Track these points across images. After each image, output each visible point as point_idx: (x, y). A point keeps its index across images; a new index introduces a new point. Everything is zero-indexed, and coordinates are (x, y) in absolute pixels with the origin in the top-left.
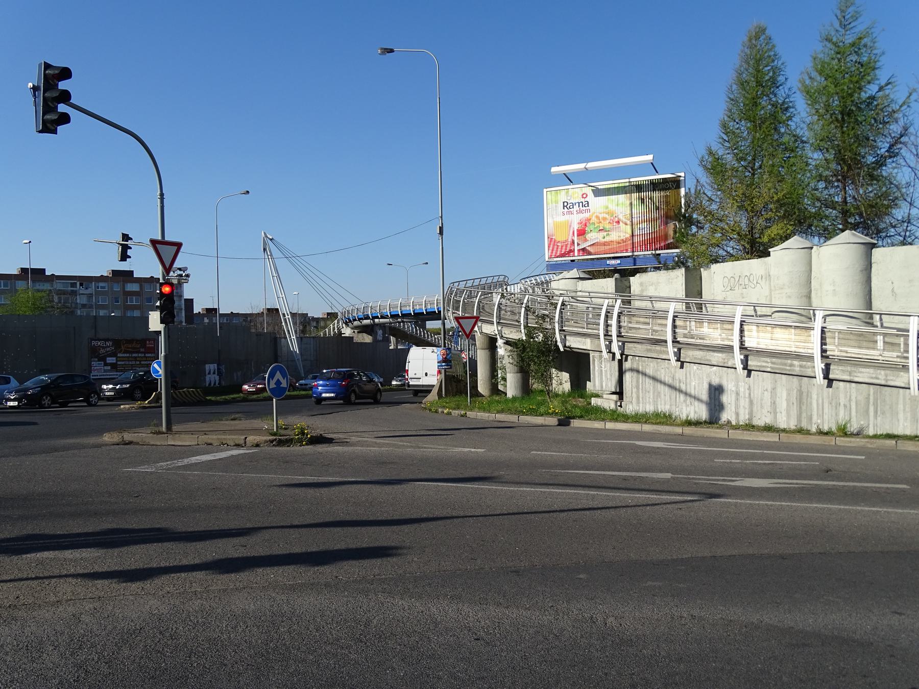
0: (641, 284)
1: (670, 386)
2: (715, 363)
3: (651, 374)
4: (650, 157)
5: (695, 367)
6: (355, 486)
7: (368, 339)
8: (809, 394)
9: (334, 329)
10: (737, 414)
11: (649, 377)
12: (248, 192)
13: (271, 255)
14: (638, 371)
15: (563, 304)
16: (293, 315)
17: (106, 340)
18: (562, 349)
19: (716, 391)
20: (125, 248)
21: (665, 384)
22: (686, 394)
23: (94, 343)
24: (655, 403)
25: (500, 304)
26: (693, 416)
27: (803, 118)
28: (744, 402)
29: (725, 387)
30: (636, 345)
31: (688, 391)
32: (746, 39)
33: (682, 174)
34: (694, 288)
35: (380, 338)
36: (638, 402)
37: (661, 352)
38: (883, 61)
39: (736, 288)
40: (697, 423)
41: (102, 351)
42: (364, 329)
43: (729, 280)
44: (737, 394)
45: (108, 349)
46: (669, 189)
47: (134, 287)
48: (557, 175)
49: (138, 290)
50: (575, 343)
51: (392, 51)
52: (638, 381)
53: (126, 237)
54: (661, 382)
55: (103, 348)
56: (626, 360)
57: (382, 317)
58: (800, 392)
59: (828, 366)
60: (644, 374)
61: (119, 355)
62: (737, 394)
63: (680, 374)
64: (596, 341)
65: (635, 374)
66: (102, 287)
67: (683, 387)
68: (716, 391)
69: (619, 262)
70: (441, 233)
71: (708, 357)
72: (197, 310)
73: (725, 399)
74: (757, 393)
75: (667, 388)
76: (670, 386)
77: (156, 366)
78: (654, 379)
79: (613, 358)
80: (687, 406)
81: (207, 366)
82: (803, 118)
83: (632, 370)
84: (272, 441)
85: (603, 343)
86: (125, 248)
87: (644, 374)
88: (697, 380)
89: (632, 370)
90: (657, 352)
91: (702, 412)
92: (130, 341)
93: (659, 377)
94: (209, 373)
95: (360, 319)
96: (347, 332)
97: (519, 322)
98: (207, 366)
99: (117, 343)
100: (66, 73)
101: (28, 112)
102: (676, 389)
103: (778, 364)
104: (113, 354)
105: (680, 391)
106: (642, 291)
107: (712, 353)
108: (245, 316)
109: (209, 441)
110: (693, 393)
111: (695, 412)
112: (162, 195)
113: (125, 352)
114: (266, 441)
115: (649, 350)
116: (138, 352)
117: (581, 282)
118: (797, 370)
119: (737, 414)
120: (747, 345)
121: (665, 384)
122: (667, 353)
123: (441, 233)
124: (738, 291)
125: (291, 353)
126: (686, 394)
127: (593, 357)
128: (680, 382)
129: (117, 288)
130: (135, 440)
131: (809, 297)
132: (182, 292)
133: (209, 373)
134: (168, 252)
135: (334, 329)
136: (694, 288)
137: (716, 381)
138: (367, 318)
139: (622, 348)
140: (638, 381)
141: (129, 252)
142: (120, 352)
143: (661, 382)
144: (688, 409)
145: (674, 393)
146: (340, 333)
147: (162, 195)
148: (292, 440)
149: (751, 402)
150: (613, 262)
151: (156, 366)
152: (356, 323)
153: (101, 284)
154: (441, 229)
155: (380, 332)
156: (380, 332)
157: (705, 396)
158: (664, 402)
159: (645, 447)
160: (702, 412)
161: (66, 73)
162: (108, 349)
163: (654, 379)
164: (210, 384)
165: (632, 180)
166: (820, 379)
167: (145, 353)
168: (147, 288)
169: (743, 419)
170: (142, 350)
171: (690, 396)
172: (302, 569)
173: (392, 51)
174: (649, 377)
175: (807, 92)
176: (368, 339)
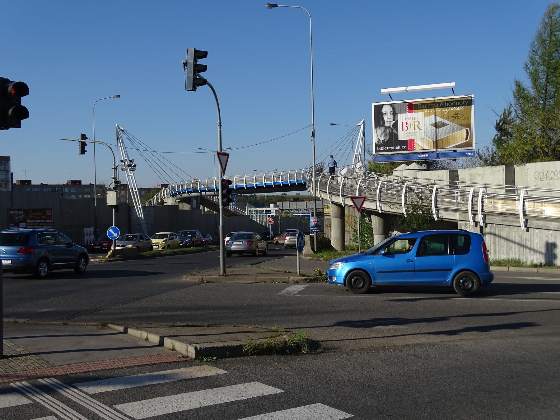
0: (471, 175)
1: (519, 244)
2: (552, 229)
3: (505, 236)
4: (453, 84)
5: (537, 231)
6: (423, 301)
7: (186, 207)
9: (157, 199)
11: (504, 238)
12: (119, 96)
13: (123, 143)
14: (495, 235)
15: (437, 190)
16: (140, 190)
18: (436, 219)
19: (551, 247)
20: (83, 145)
21: (515, 243)
22: (530, 249)
23: (11, 212)
24: (508, 254)
25: (344, 184)
26: (536, 262)
30: (494, 217)
31: (532, 247)
33: (473, 96)
34: (510, 179)
35: (194, 206)
36: (495, 253)
37: (515, 221)
39: (545, 179)
40: (541, 266)
41: (17, 218)
42: (187, 200)
43: (539, 174)
45: (21, 217)
46: (462, 105)
48: (385, 94)
50: (446, 215)
51: (276, 6)
52: (495, 240)
53: (84, 137)
54: (512, 241)
55: (18, 216)
56: (486, 226)
57: (209, 191)
60: (500, 237)
61: (28, 221)
63: (526, 235)
64: (464, 214)
65: (493, 237)
67: (529, 245)
68: (551, 247)
69: (427, 155)
70: (313, 136)
71: (547, 225)
72: (15, 182)
75: (516, 246)
76: (519, 244)
77: (111, 230)
78: (507, 240)
79: (476, 225)
80: (531, 255)
81: (85, 229)
83: (490, 233)
84: (306, 280)
85: (470, 215)
86: (83, 145)
87: (500, 237)
88: (538, 239)
89: (490, 233)
90: (510, 221)
91: (540, 259)
92: (36, 211)
93: (510, 238)
94: (87, 235)
95: (188, 192)
96: (169, 201)
98: (85, 229)
100: (204, 55)
101: (182, 77)
102: (523, 246)
105: (526, 247)
106: (471, 179)
107: (550, 222)
108: (54, 187)
109: (264, 280)
110: (536, 248)
111: (537, 259)
112: (220, 123)
113: (32, 219)
114: (303, 280)
115: (505, 220)
116: (41, 219)
117: (420, 172)
120: (485, 210)
121: (515, 243)
122: (519, 222)
123: (313, 136)
124: (546, 181)
125: (139, 219)
126: (530, 249)
127: (461, 224)
128: (526, 240)
130: (211, 280)
132: (9, 167)
133: (87, 235)
134: (223, 158)
135: (157, 199)
136: (510, 179)
137: (551, 240)
138: (196, 191)
139: (484, 219)
140: (495, 240)
141: (87, 148)
142: (28, 219)
143: (512, 241)
144: (532, 257)
145: (521, 249)
146: (162, 202)
147: (220, 123)
148: (317, 279)
150: (423, 156)
151: (111, 230)
152: (179, 196)
154: (313, 133)
155: (195, 201)
156: (195, 201)
157: (543, 250)
158: (515, 254)
159: (526, 279)
160: (540, 259)
161: (204, 55)
162: (21, 217)
163: (507, 240)
164: (87, 243)
165: (436, 99)
167: (45, 219)
170: (43, 217)
171: (534, 250)
172: (509, 330)
173: (276, 6)
174: (504, 238)
176: (186, 207)
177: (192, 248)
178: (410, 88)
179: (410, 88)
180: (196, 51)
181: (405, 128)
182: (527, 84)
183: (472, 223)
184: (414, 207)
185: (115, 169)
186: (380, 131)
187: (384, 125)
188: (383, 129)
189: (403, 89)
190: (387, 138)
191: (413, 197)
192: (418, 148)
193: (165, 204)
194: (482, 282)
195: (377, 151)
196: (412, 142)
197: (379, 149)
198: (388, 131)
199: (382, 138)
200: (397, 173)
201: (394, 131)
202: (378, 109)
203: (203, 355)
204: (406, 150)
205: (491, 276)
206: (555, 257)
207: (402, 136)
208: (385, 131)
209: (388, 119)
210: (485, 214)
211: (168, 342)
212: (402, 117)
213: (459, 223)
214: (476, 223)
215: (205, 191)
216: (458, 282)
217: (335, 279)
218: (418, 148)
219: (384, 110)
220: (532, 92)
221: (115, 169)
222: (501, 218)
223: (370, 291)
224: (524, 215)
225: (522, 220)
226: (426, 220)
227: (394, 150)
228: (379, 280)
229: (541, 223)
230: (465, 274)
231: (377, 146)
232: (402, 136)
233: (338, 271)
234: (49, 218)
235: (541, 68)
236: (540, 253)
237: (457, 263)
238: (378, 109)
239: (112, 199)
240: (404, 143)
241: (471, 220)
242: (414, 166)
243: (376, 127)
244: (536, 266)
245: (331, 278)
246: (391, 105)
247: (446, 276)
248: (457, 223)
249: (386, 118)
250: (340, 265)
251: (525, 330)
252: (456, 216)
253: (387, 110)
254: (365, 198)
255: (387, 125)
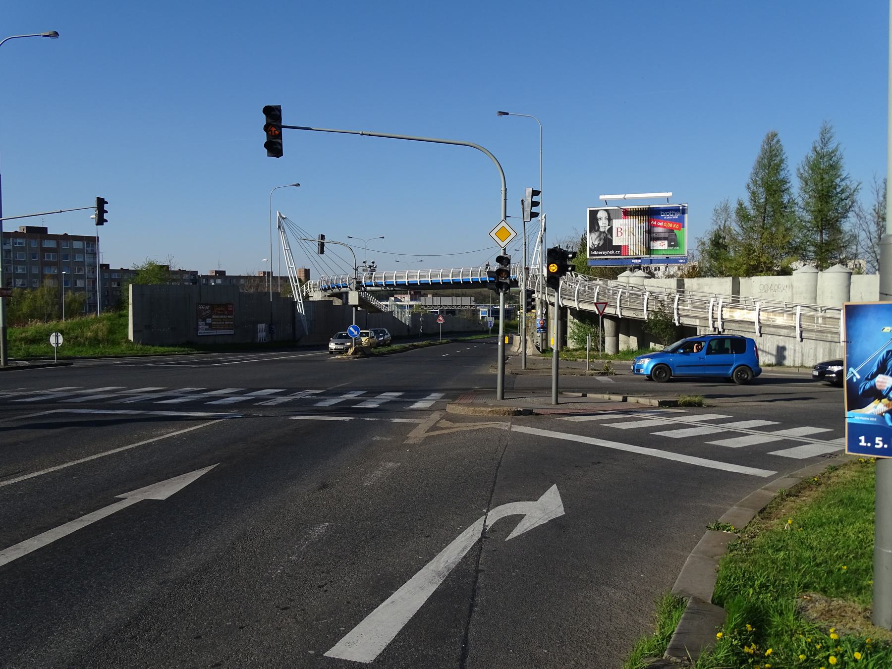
0: (698, 284)
4: (670, 194)
8: (835, 351)
10: (794, 361)
17: (206, 304)
18: (677, 324)
19: (781, 350)
26: (770, 362)
27: (797, 191)
28: (798, 355)
29: (787, 347)
32: (765, 138)
34: (736, 290)
38: (842, 162)
44: (795, 350)
47: (52, 244)
49: (55, 246)
50: (686, 321)
51: (507, 114)
57: (376, 286)
58: (830, 349)
59: (760, 327)
62: (795, 350)
66: (20, 243)
68: (781, 350)
73: (787, 353)
74: (806, 350)
77: (351, 329)
82: (797, 191)
85: (711, 322)
86: (322, 245)
97: (838, 333)
99: (212, 307)
103: (819, 336)
104: (210, 317)
116: (223, 314)
118: (829, 339)
119: (794, 361)
129: (34, 244)
131: (815, 299)
136: (736, 290)
137: (781, 345)
149: (803, 355)
150: (636, 261)
151: (351, 329)
153: (18, 240)
157: (774, 353)
160: (772, 360)
166: (799, 339)
168: (64, 245)
169: (798, 363)
173: (507, 114)
175: (801, 177)
177: (395, 346)
178: (628, 196)
179: (628, 196)
180: (533, 191)
181: (620, 234)
182: (747, 204)
183: (711, 329)
184: (655, 313)
185: (356, 269)
186: (595, 235)
187: (598, 230)
188: (597, 233)
189: (622, 196)
190: (601, 243)
191: (655, 307)
192: (631, 254)
193: (311, 299)
194: (751, 375)
195: (591, 255)
196: (626, 247)
197: (593, 253)
198: (602, 236)
199: (596, 243)
200: (622, 278)
201: (609, 236)
202: (593, 214)
203: (662, 404)
204: (620, 255)
205: (760, 371)
206: (784, 358)
207: (616, 242)
208: (599, 236)
209: (603, 224)
210: (724, 321)
211: (631, 399)
212: (617, 223)
213: (698, 328)
214: (715, 329)
215: (371, 286)
216: (737, 374)
217: (642, 371)
218: (631, 254)
219: (599, 215)
220: (752, 212)
221: (356, 269)
222: (738, 325)
223: (670, 381)
224: (759, 322)
225: (757, 327)
226: (668, 323)
227: (607, 255)
228: (678, 372)
229: (773, 330)
230: (743, 368)
231: (591, 250)
232: (616, 242)
233: (645, 366)
234: (231, 313)
235: (761, 189)
236: (771, 354)
237: (736, 359)
238: (593, 214)
239: (353, 298)
240: (618, 248)
241: (711, 326)
242: (640, 273)
243: (590, 231)
244: (769, 365)
245: (638, 370)
246: (606, 210)
247: (728, 370)
248: (696, 329)
249: (600, 223)
250: (647, 361)
251: (810, 401)
252: (697, 322)
253: (602, 215)
254: (606, 303)
255: (602, 230)
